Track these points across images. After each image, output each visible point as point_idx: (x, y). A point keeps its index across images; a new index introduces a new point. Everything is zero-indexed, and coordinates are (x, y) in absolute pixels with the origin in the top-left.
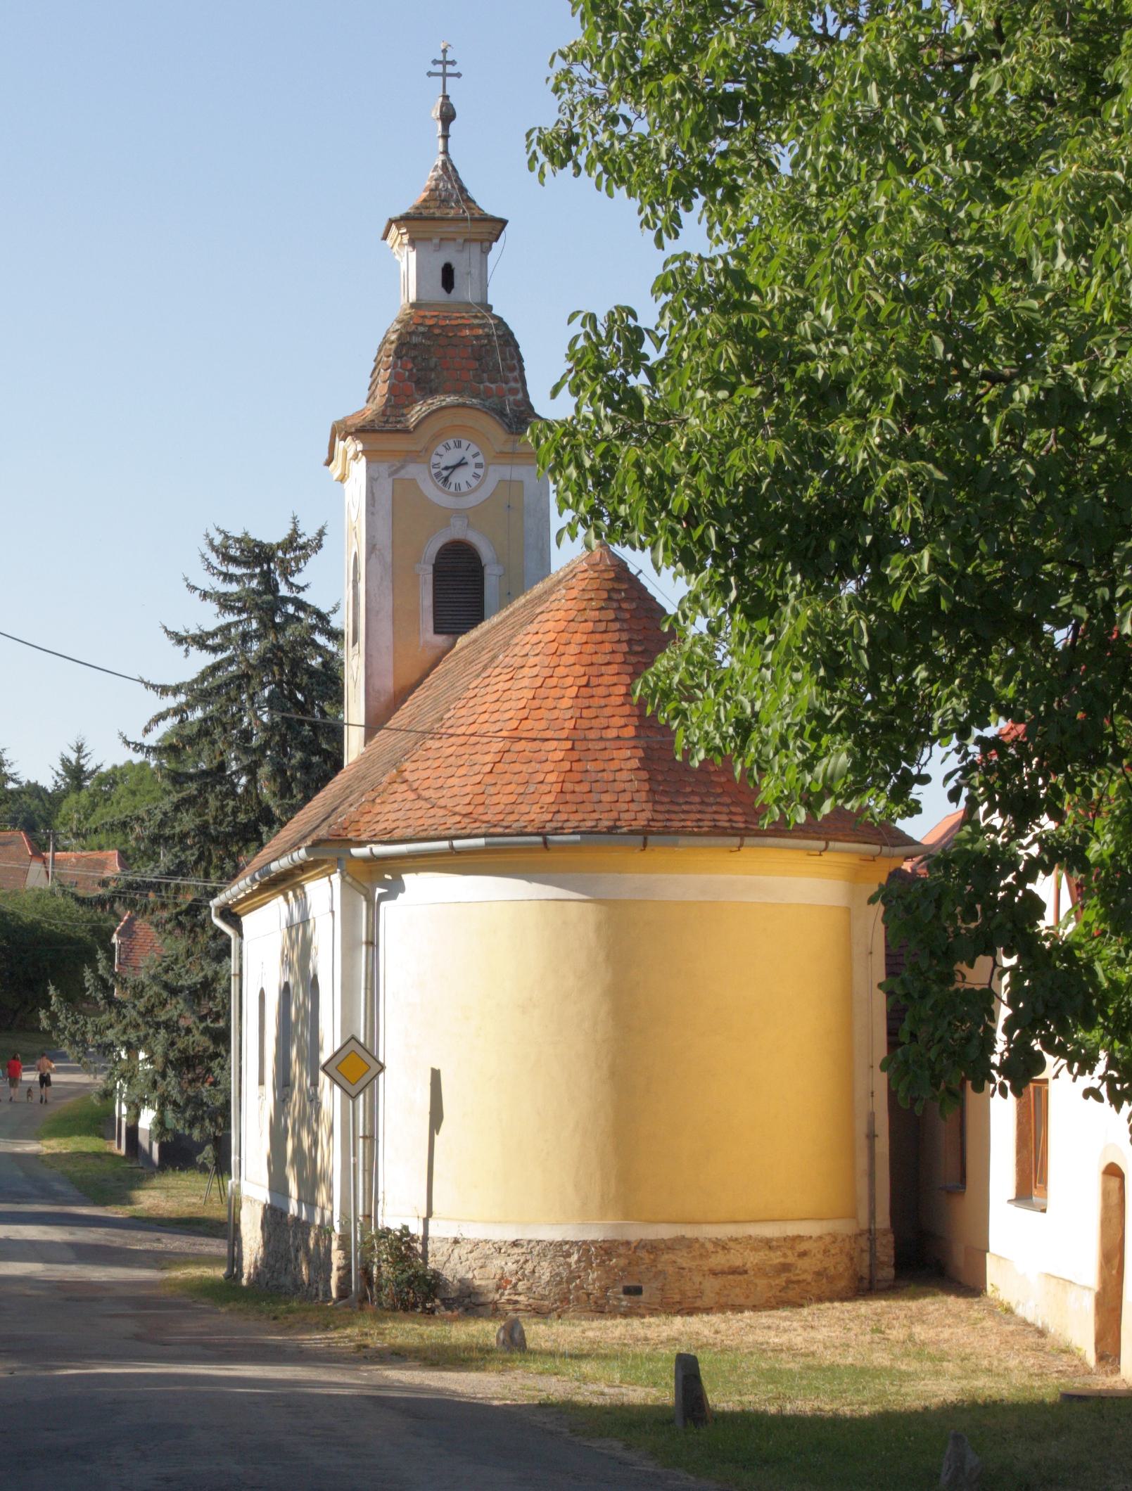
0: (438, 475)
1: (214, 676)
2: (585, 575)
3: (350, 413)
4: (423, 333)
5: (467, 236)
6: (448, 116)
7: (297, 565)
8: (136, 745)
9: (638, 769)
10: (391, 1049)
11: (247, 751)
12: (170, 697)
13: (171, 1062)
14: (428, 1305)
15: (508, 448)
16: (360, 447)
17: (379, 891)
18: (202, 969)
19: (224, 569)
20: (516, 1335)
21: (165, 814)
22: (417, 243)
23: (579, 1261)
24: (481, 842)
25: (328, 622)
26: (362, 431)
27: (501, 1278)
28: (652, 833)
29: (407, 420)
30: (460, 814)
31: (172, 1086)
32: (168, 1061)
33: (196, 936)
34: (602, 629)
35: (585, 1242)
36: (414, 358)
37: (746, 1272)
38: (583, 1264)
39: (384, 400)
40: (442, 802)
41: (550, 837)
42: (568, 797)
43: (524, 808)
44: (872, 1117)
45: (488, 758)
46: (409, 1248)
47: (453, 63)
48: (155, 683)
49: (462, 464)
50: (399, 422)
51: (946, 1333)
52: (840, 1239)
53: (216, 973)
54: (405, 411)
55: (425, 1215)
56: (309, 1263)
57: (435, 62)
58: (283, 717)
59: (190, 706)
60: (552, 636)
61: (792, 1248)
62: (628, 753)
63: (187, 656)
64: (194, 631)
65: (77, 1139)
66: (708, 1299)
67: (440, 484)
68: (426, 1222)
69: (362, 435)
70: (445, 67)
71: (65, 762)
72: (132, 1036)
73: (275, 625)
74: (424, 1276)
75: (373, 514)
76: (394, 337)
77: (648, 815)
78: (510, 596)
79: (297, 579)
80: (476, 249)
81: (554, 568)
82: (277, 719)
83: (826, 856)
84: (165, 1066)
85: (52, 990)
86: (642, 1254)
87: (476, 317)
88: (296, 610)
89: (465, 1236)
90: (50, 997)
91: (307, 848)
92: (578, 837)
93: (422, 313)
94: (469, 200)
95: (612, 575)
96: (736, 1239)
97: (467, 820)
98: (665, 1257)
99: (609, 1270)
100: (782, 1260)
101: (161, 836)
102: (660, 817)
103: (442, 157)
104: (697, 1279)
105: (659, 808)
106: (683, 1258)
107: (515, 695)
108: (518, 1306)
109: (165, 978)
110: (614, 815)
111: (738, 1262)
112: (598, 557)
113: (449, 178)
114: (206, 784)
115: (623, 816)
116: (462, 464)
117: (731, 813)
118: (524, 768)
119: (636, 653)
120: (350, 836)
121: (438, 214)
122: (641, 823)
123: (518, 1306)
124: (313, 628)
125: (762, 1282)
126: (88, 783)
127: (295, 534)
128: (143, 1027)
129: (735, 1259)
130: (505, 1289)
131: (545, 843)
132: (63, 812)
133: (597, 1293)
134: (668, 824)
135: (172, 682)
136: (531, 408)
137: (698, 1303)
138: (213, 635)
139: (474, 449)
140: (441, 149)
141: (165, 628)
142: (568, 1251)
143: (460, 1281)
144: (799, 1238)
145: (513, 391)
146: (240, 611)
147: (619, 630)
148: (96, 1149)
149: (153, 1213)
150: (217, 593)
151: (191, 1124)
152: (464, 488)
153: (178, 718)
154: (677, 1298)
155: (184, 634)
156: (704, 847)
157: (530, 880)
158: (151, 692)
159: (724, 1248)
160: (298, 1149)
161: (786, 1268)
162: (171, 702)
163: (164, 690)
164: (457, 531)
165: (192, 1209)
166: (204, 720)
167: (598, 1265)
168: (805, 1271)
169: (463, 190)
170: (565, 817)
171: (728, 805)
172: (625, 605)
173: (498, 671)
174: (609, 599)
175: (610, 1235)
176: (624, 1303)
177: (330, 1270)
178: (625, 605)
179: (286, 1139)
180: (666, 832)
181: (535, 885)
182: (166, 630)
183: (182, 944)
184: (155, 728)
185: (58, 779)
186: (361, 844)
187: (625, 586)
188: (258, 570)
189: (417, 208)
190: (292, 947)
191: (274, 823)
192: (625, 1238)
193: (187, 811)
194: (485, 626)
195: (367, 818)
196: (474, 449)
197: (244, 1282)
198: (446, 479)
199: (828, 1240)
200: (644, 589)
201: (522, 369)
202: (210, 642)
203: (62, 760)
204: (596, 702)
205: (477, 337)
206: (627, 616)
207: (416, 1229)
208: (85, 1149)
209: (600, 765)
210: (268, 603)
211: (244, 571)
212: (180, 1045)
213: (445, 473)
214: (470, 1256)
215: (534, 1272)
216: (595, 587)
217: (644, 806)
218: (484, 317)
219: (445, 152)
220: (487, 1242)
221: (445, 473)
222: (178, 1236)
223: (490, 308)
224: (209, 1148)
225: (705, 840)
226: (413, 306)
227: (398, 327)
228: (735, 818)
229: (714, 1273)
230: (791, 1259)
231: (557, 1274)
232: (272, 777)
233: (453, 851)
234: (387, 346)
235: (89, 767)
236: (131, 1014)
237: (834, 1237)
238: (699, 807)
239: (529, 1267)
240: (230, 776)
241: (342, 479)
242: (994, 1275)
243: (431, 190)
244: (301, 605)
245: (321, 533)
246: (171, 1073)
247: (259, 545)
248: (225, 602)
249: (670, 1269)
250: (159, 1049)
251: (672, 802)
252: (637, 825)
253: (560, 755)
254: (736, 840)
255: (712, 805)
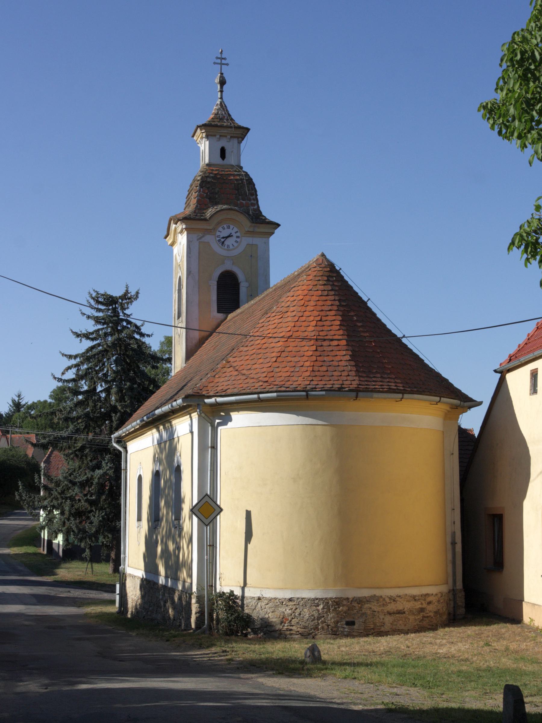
0: (219, 241)
1: (92, 351)
2: (315, 269)
3: (178, 213)
4: (212, 177)
5: (232, 135)
6: (223, 82)
7: (128, 306)
8: (59, 379)
9: (350, 360)
10: (222, 499)
11: (106, 382)
12: (73, 360)
13: (72, 514)
14: (244, 632)
15: (251, 230)
16: (184, 226)
17: (217, 421)
18: (86, 474)
19: (97, 307)
20: (316, 653)
21: (71, 408)
22: (209, 137)
23: (323, 608)
24: (275, 394)
25: (140, 330)
26: (185, 219)
27: (283, 618)
28: (360, 391)
29: (205, 215)
30: (262, 381)
31: (73, 523)
32: (70, 514)
33: (83, 461)
34: (326, 294)
35: (326, 599)
36: (208, 188)
37: (404, 613)
38: (325, 610)
39: (195, 206)
40: (252, 376)
41: (309, 393)
42: (317, 373)
43: (295, 379)
44: (454, 534)
45: (274, 355)
46: (234, 602)
47: (225, 59)
48: (66, 354)
49: (230, 236)
50: (202, 216)
51: (523, 646)
52: (444, 594)
53: (92, 476)
54: (204, 211)
55: (242, 585)
56: (174, 609)
57: (217, 58)
58: (122, 368)
59: (82, 363)
60: (301, 297)
61: (425, 600)
62: (344, 353)
63: (81, 342)
64: (84, 332)
65: (25, 547)
66: (387, 628)
67: (220, 245)
68: (243, 589)
69: (186, 221)
70: (221, 61)
71: (13, 401)
72: (55, 503)
73: (118, 330)
74: (242, 616)
75: (190, 257)
76: (199, 178)
77: (357, 382)
78: (251, 296)
79: (127, 312)
80: (235, 141)
81: (271, 286)
82: (119, 369)
83: (440, 405)
84: (70, 516)
85: (20, 483)
86: (355, 604)
87: (236, 171)
88: (127, 324)
89: (264, 596)
90: (19, 487)
91: (183, 399)
92: (324, 393)
93: (212, 168)
94: (232, 119)
95: (328, 269)
96: (400, 596)
97: (266, 384)
98: (367, 606)
99: (338, 613)
100: (420, 606)
101: (69, 418)
102: (363, 383)
103: (219, 100)
104: (382, 617)
105: (361, 379)
106: (375, 606)
107: (285, 325)
108: (292, 632)
109: (70, 478)
110: (340, 382)
111: (400, 608)
112: (321, 261)
113: (223, 109)
114: (89, 396)
115: (345, 382)
116: (230, 236)
117: (395, 382)
118: (293, 359)
119: (343, 306)
120: (204, 393)
121: (219, 124)
122: (354, 385)
123: (292, 632)
124: (134, 331)
125: (412, 618)
126: (22, 409)
127: (127, 292)
128: (60, 499)
129: (399, 606)
130: (285, 623)
131: (307, 395)
132: (13, 419)
133: (333, 625)
134: (368, 387)
135: (74, 353)
136: (261, 213)
137: (382, 629)
138: (92, 333)
139: (236, 229)
140: (219, 96)
141: (71, 330)
142: (317, 603)
143: (261, 619)
144: (427, 595)
145: (253, 205)
146: (104, 324)
147: (334, 295)
148: (34, 552)
149: (64, 579)
150: (94, 316)
151: (81, 540)
152: (231, 247)
153: (77, 368)
154: (372, 626)
155: (80, 333)
156: (385, 398)
157: (298, 415)
158: (65, 358)
159: (394, 601)
160: (165, 551)
161: (422, 610)
162: (73, 362)
163: (70, 357)
164: (228, 266)
165: (79, 577)
166: (88, 369)
167: (333, 610)
168: (430, 611)
169: (229, 115)
170: (316, 383)
171: (394, 379)
172: (336, 284)
173: (274, 314)
174: (328, 280)
175: (339, 595)
176: (346, 630)
177: (191, 613)
178: (336, 284)
179: (157, 546)
180: (367, 390)
181: (300, 417)
182: (72, 331)
183: (77, 463)
184: (66, 373)
185: (10, 407)
186: (209, 397)
187: (335, 275)
188: (111, 307)
189: (209, 122)
190: (161, 452)
191: (117, 412)
192: (346, 597)
193: (80, 407)
194: (238, 311)
195: (212, 384)
196: (236, 229)
197: (129, 616)
198: (223, 242)
199: (439, 595)
200: (343, 277)
201: (257, 195)
202: (91, 336)
203: (12, 400)
204: (326, 328)
205: (237, 180)
206: (337, 288)
207: (238, 592)
208: (29, 552)
209: (330, 358)
210: (115, 320)
211: (105, 307)
212: (76, 506)
213: (223, 240)
214: (267, 606)
215: (300, 614)
216: (321, 274)
217: (355, 378)
218: (239, 171)
219: (221, 98)
220: (275, 599)
221: (223, 240)
222: (77, 590)
223: (241, 168)
224: (87, 550)
225: (386, 395)
226: (207, 165)
227: (201, 174)
228: (398, 385)
229: (390, 613)
230: (424, 606)
231: (312, 615)
232: (117, 393)
233: (260, 400)
234: (196, 182)
235: (23, 403)
236: (55, 493)
237: (441, 593)
238: (380, 379)
239: (298, 611)
240: (99, 392)
241: (173, 244)
242: (528, 614)
243: (215, 114)
244: (129, 322)
245: (137, 293)
246: (72, 519)
247: (111, 297)
248: (97, 320)
249: (369, 612)
250: (67, 509)
251: (367, 377)
252: (352, 387)
253: (310, 353)
254: (400, 396)
255: (386, 378)
